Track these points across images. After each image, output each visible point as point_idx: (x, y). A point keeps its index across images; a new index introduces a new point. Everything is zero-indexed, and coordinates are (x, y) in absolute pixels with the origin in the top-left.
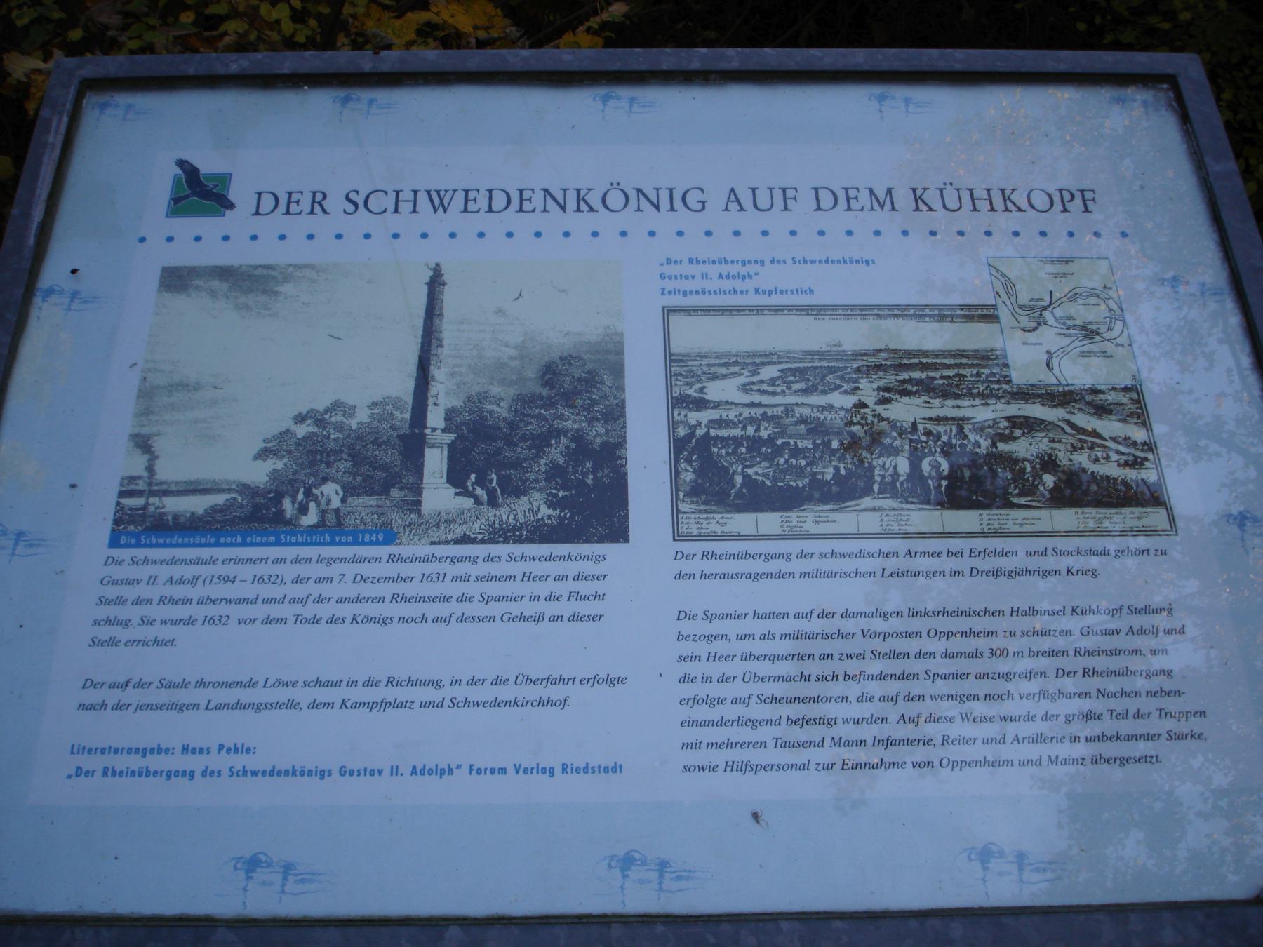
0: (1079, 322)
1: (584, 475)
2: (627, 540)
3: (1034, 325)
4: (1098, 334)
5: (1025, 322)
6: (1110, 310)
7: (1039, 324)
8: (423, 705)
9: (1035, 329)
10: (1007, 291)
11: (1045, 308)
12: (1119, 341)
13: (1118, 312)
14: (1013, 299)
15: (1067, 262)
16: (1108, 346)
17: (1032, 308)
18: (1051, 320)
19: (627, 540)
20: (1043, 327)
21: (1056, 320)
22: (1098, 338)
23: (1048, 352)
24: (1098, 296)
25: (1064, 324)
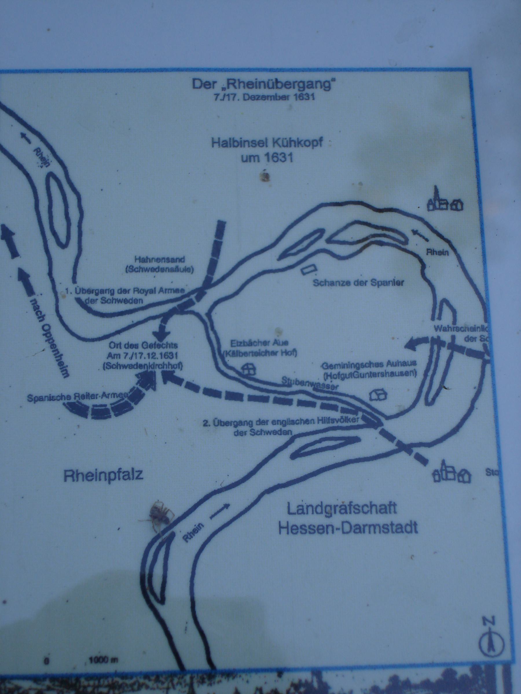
0: (307, 369)
1: (89, 686)
2: (225, 223)
3: (125, 381)
4: (373, 420)
5: (94, 375)
6: (439, 306)
7: (147, 380)
8: (23, 276)
9: (124, 405)
10: (45, 229)
11: (183, 305)
12: (450, 453)
13: (470, 313)
14: (63, 259)
15: (304, 90)
16: (398, 481)
17: (129, 303)
18: (195, 361)
19: (225, 223)
20: (164, 393)
21: (218, 355)
22: (371, 441)
23: (158, 515)
24: (401, 244)
25: (246, 375)
